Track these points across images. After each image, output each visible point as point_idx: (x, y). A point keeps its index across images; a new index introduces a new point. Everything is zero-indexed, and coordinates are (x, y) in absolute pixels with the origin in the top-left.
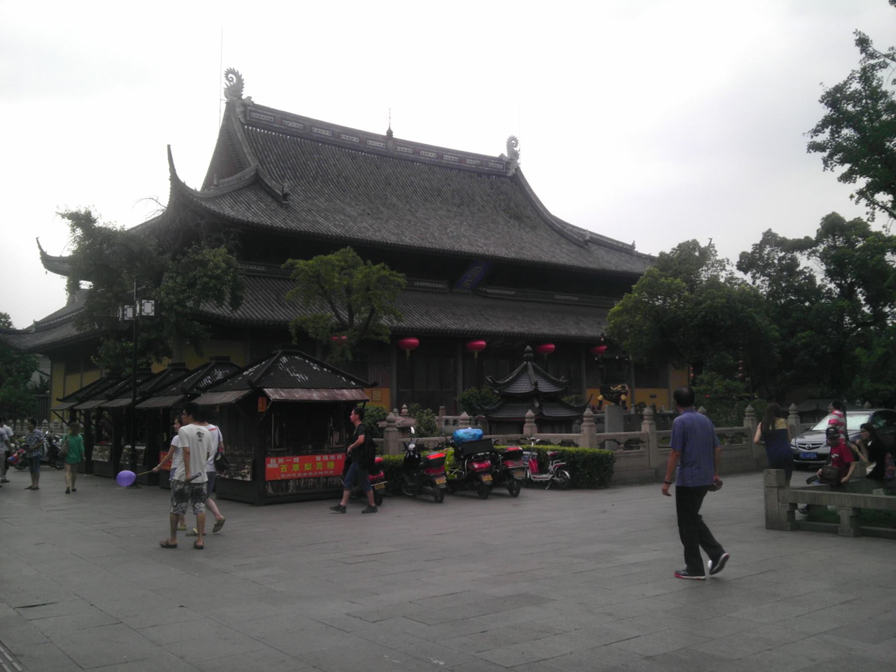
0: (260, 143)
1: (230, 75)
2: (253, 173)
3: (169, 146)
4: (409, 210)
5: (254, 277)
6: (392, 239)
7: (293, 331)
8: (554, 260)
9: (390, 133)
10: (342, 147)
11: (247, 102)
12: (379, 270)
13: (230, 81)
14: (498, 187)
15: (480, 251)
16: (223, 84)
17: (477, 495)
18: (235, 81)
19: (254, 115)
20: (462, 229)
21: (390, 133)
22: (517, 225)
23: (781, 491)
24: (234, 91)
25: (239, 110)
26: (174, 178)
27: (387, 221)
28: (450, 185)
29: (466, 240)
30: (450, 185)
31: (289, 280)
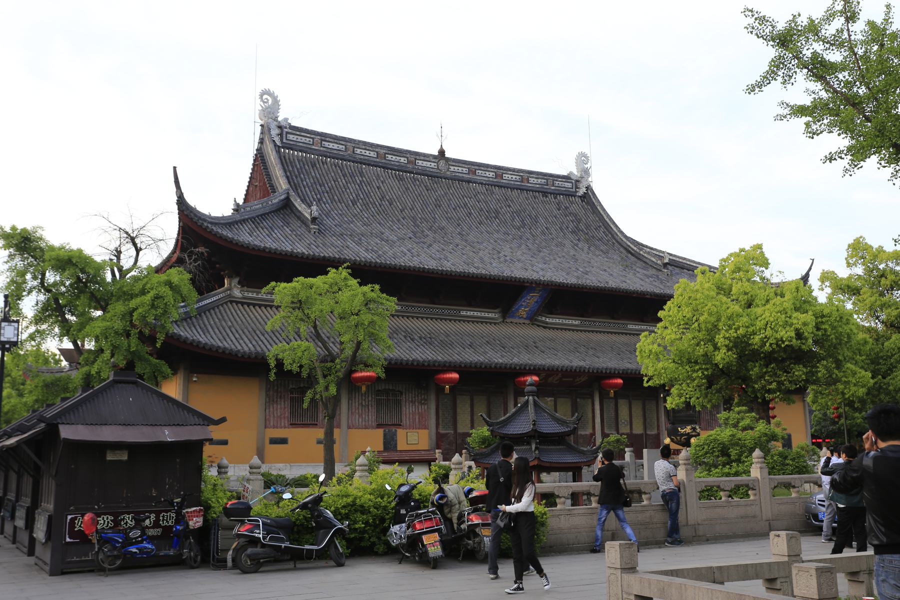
0: (294, 161)
1: (265, 97)
2: (283, 197)
3: (175, 168)
4: (460, 234)
5: (266, 306)
6: (430, 264)
7: (272, 363)
8: (624, 286)
9: (442, 152)
10: (434, 177)
11: (284, 124)
12: (371, 291)
13: (264, 102)
14: (566, 208)
15: (535, 276)
16: (258, 105)
17: (333, 564)
18: (270, 102)
19: (291, 137)
20: (519, 253)
21: (442, 152)
22: (586, 249)
23: (625, 576)
24: (270, 110)
25: (275, 132)
26: (181, 202)
27: (430, 245)
28: (510, 206)
29: (521, 265)
30: (510, 206)
31: (271, 307)
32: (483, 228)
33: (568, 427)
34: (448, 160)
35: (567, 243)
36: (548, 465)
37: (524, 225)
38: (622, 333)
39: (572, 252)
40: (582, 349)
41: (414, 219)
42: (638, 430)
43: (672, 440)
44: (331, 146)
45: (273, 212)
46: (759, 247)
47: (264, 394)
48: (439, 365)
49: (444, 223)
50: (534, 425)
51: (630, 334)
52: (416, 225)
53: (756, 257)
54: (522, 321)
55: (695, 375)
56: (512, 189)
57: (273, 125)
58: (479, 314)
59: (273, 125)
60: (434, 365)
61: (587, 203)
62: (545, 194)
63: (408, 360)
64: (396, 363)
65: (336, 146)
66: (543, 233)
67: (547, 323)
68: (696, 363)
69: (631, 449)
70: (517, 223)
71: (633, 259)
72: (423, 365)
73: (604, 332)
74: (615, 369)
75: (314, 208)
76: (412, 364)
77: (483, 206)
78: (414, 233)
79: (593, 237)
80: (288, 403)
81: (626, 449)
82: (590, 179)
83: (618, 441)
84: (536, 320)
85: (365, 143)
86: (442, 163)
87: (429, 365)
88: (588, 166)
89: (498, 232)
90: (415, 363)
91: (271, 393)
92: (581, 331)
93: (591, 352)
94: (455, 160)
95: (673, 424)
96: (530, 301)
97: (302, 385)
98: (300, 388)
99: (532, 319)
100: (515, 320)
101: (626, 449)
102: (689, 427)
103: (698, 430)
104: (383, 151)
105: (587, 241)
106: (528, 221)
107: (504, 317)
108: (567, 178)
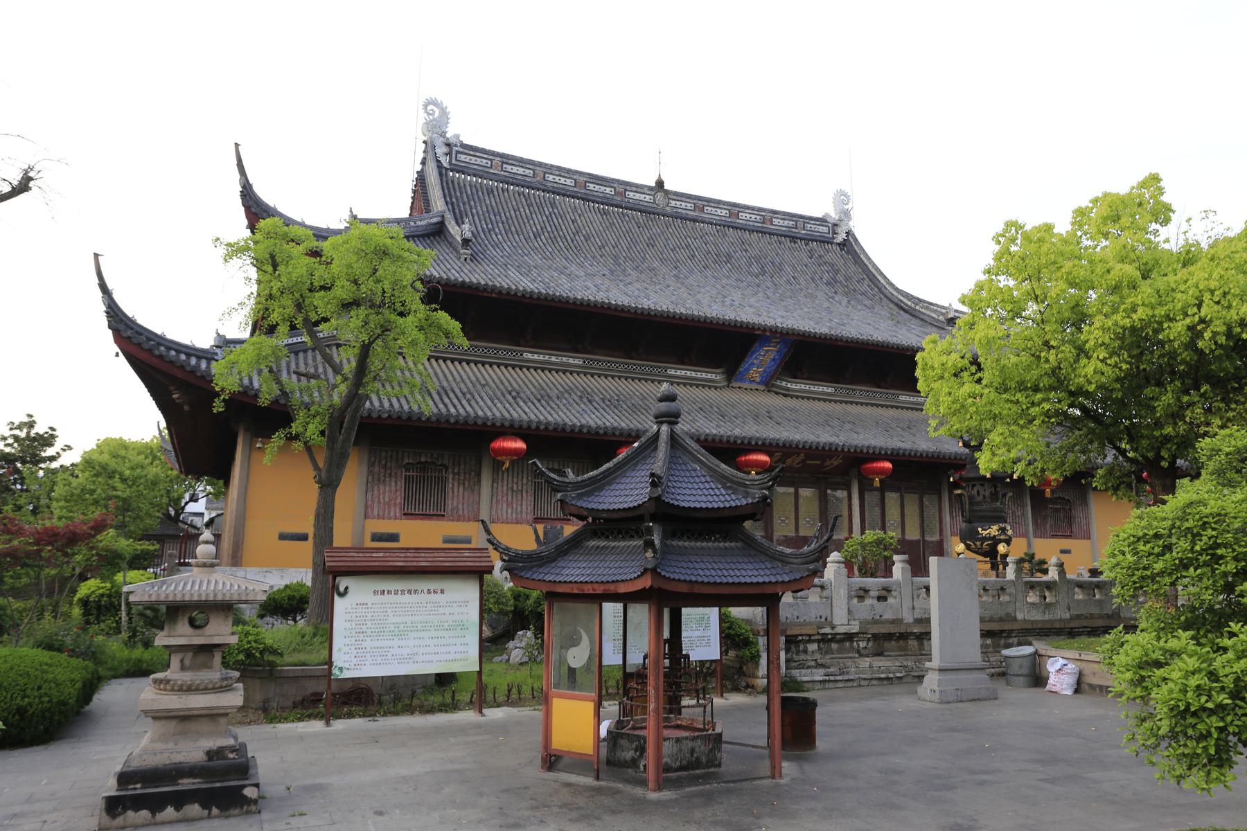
0: (461, 181)
1: (430, 107)
2: (434, 220)
9: (660, 183)
11: (453, 141)
13: (429, 114)
16: (422, 117)
18: (437, 114)
19: (462, 157)
21: (660, 183)
25: (441, 150)
28: (746, 251)
29: (752, 310)
30: (746, 251)
32: (709, 273)
33: (747, 495)
34: (667, 192)
35: (820, 295)
36: (684, 589)
37: (763, 273)
38: (892, 407)
39: (826, 304)
40: (836, 422)
41: (616, 258)
42: (913, 534)
43: (968, 547)
44: (515, 170)
45: (418, 236)
46: (1154, 180)
47: (364, 468)
48: (621, 434)
49: (656, 264)
50: (654, 484)
51: (902, 408)
52: (616, 263)
53: (1147, 204)
54: (754, 386)
55: (1034, 411)
56: (751, 231)
57: (439, 142)
58: (693, 374)
59: (439, 142)
60: (614, 434)
61: (848, 252)
62: (793, 239)
63: (574, 425)
64: (555, 429)
65: (521, 171)
66: (789, 282)
67: (788, 389)
68: (1036, 389)
69: (905, 557)
70: (755, 269)
71: (906, 316)
72: (597, 433)
73: (867, 404)
74: (881, 448)
75: (466, 227)
76: (580, 431)
77: (711, 248)
78: (612, 272)
79: (855, 291)
80: (401, 484)
81: (895, 558)
82: (851, 223)
83: (879, 542)
84: (773, 385)
85: (559, 168)
86: (660, 196)
87: (605, 433)
88: (849, 207)
89: (728, 278)
90: (585, 431)
91: (376, 469)
92: (836, 402)
93: (847, 426)
94: (676, 194)
95: (969, 521)
96: (763, 358)
97: (423, 460)
98: (420, 463)
99: (768, 384)
100: (744, 385)
101: (895, 558)
102: (995, 527)
103: (1010, 532)
104: (582, 179)
105: (846, 294)
106: (769, 268)
107: (729, 380)
108: (822, 221)
